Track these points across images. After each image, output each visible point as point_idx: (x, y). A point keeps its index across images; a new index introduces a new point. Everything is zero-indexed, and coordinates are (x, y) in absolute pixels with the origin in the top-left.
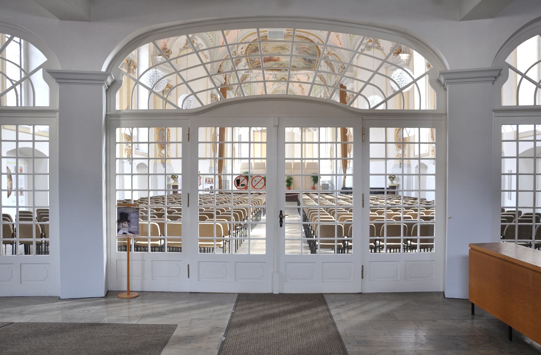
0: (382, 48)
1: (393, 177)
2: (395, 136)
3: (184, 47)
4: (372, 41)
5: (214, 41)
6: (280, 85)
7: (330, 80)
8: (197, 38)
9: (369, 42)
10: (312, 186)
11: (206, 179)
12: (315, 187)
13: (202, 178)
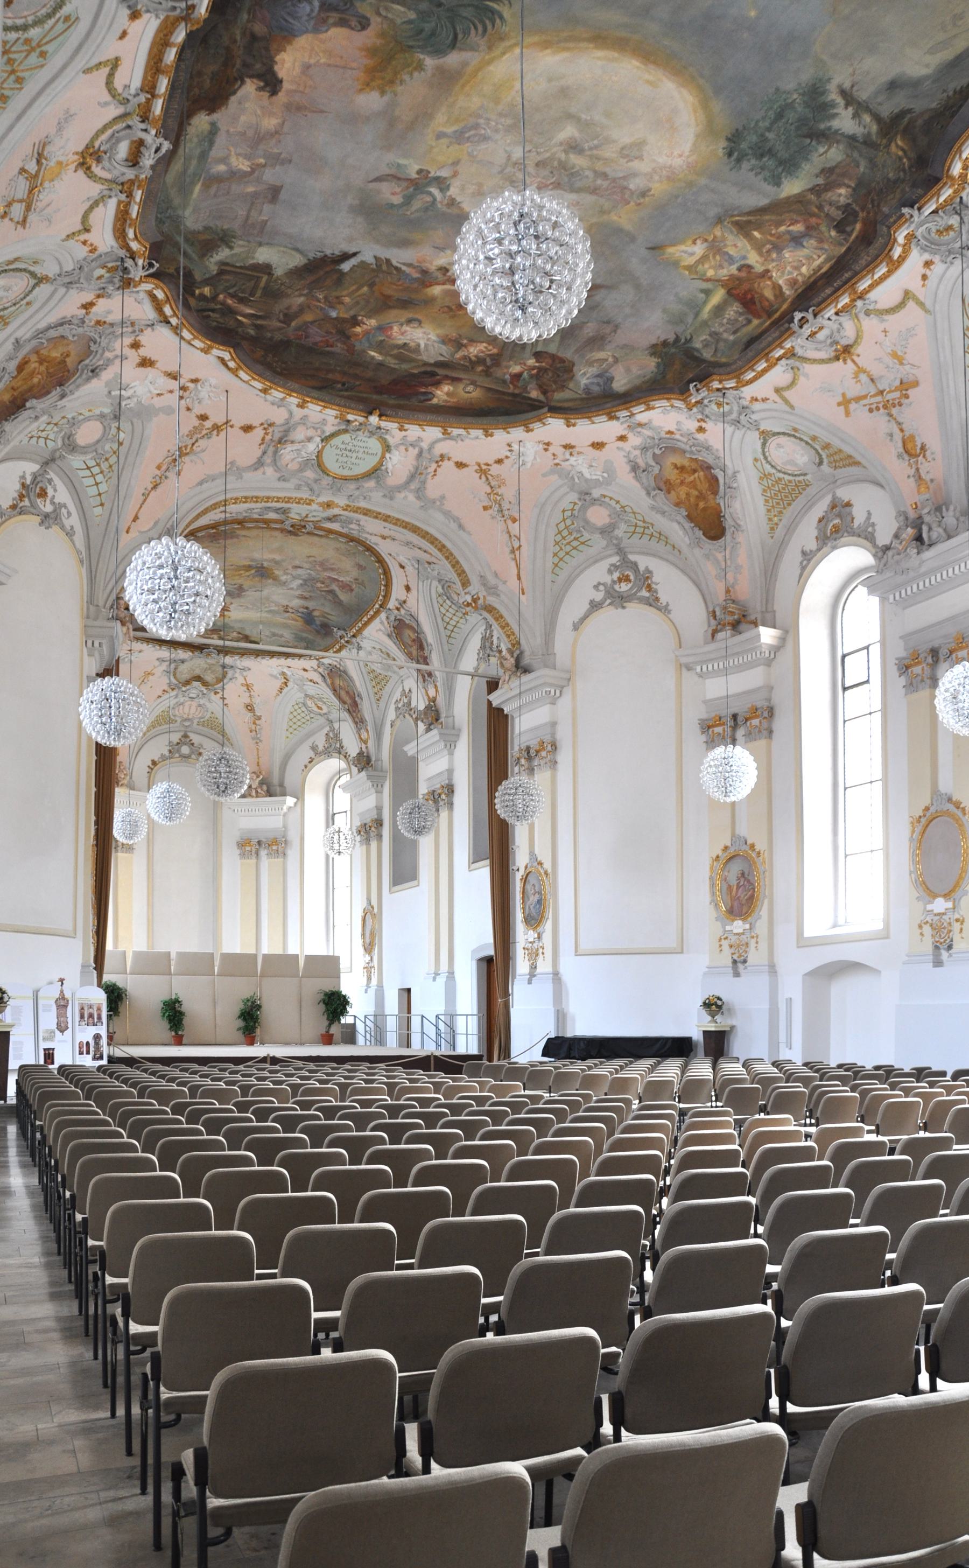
0: (664, 604)
1: (719, 1003)
2: (711, 878)
3: (14, 507)
4: (630, 581)
5: (108, 506)
6: (182, 700)
7: (377, 697)
8: (57, 481)
9: (620, 580)
10: (323, 1031)
11: (82, 1009)
12: (332, 1035)
13: (70, 1002)
